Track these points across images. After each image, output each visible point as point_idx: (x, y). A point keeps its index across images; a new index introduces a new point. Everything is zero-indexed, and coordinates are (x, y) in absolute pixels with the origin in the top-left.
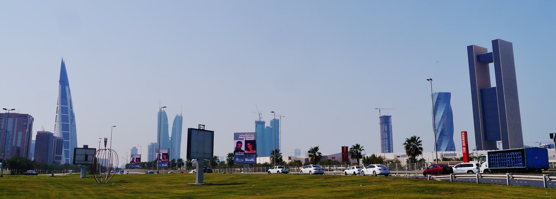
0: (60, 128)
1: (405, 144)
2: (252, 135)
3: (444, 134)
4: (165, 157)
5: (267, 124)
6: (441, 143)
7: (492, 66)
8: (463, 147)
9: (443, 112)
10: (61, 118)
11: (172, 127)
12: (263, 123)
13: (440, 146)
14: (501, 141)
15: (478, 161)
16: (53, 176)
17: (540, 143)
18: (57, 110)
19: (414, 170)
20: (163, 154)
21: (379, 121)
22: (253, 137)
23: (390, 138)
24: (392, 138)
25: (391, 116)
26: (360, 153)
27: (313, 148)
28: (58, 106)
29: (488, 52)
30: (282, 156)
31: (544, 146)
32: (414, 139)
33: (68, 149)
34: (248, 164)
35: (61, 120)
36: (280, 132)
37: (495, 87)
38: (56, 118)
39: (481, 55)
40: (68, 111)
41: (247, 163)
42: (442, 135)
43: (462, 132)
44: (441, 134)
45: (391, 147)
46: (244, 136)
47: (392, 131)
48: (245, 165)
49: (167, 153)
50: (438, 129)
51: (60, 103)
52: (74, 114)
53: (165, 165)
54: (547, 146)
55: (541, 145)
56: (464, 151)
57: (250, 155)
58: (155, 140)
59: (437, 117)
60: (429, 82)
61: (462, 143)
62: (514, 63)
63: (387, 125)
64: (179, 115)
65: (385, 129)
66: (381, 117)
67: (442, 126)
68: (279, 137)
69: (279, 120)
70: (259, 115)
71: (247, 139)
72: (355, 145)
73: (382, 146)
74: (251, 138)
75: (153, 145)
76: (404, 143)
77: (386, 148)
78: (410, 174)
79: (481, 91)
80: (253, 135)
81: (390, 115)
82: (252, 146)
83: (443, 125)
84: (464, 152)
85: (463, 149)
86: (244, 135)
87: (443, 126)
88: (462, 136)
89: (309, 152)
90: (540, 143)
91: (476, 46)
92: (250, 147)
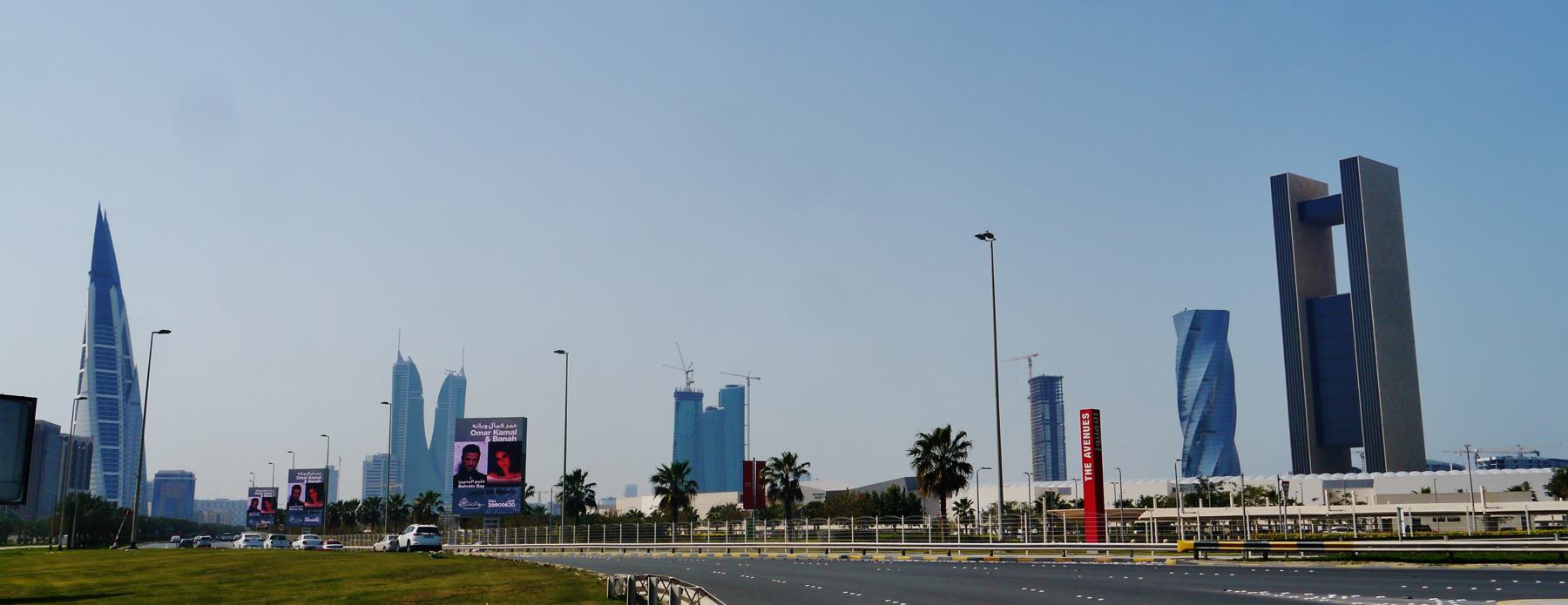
0: (90, 410)
1: (915, 452)
2: (511, 426)
3: (1209, 429)
4: (314, 495)
5: (711, 400)
6: (1201, 455)
7: (1339, 233)
8: (1085, 460)
10: (93, 382)
11: (436, 410)
12: (699, 396)
13: (1198, 464)
14: (1362, 449)
16: (395, 544)
17: (1477, 455)
18: (83, 356)
19: (504, 543)
20: (307, 484)
21: (1026, 391)
22: (515, 432)
23: (1059, 441)
24: (1064, 440)
25: (1062, 377)
26: (795, 482)
27: (669, 467)
28: (86, 345)
29: (1330, 194)
30: (593, 492)
31: (1485, 462)
32: (942, 436)
33: (115, 474)
34: (497, 515)
35: (93, 386)
36: (746, 423)
37: (1348, 295)
38: (80, 382)
39: (1311, 201)
40: (114, 359)
41: (492, 515)
42: (1204, 431)
43: (1083, 412)
44: (1201, 430)
45: (1061, 464)
46: (488, 430)
47: (1063, 418)
48: (487, 521)
49: (320, 481)
50: (1192, 413)
51: (92, 337)
52: (136, 371)
53: (314, 520)
54: (1494, 462)
55: (1478, 460)
56: (1088, 476)
57: (503, 489)
58: (381, 445)
59: (1189, 380)
60: (986, 244)
61: (1083, 449)
62: (1401, 225)
63: (1050, 404)
64: (455, 374)
65: (1043, 414)
66: (1033, 381)
67: (1204, 405)
68: (743, 434)
69: (743, 388)
70: (687, 373)
71: (495, 439)
72: (781, 458)
73: (1037, 461)
74: (507, 436)
75: (377, 460)
76: (912, 448)
77: (1046, 470)
78: (904, 554)
79: (1310, 305)
80: (515, 426)
81: (1058, 375)
82: (511, 460)
84: (1087, 479)
85: (1084, 469)
86: (486, 427)
87: (1205, 407)
88: (1082, 426)
89: (655, 479)
90: (1477, 455)
91: (1295, 178)
92: (504, 463)
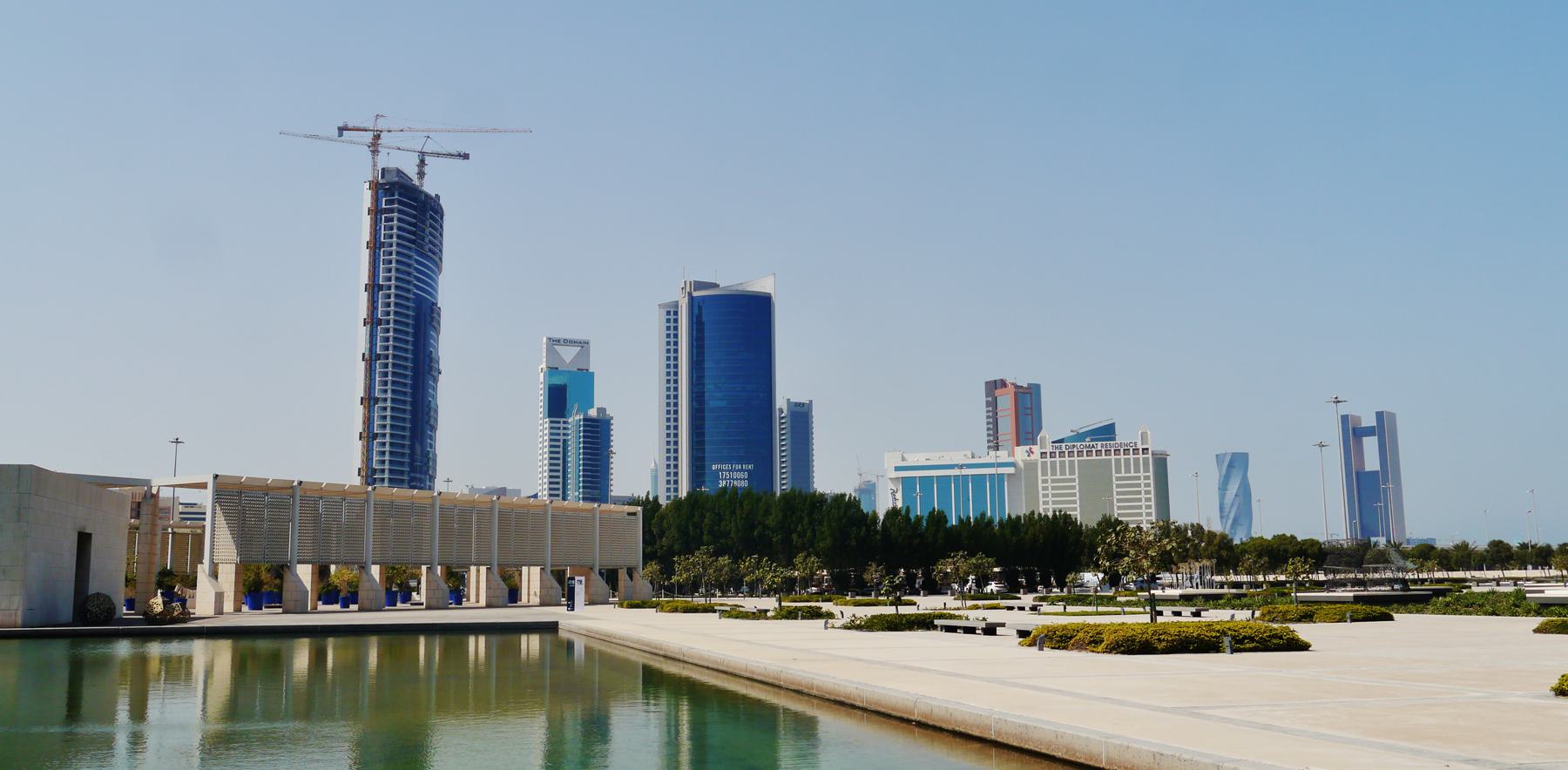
37: (1378, 472)
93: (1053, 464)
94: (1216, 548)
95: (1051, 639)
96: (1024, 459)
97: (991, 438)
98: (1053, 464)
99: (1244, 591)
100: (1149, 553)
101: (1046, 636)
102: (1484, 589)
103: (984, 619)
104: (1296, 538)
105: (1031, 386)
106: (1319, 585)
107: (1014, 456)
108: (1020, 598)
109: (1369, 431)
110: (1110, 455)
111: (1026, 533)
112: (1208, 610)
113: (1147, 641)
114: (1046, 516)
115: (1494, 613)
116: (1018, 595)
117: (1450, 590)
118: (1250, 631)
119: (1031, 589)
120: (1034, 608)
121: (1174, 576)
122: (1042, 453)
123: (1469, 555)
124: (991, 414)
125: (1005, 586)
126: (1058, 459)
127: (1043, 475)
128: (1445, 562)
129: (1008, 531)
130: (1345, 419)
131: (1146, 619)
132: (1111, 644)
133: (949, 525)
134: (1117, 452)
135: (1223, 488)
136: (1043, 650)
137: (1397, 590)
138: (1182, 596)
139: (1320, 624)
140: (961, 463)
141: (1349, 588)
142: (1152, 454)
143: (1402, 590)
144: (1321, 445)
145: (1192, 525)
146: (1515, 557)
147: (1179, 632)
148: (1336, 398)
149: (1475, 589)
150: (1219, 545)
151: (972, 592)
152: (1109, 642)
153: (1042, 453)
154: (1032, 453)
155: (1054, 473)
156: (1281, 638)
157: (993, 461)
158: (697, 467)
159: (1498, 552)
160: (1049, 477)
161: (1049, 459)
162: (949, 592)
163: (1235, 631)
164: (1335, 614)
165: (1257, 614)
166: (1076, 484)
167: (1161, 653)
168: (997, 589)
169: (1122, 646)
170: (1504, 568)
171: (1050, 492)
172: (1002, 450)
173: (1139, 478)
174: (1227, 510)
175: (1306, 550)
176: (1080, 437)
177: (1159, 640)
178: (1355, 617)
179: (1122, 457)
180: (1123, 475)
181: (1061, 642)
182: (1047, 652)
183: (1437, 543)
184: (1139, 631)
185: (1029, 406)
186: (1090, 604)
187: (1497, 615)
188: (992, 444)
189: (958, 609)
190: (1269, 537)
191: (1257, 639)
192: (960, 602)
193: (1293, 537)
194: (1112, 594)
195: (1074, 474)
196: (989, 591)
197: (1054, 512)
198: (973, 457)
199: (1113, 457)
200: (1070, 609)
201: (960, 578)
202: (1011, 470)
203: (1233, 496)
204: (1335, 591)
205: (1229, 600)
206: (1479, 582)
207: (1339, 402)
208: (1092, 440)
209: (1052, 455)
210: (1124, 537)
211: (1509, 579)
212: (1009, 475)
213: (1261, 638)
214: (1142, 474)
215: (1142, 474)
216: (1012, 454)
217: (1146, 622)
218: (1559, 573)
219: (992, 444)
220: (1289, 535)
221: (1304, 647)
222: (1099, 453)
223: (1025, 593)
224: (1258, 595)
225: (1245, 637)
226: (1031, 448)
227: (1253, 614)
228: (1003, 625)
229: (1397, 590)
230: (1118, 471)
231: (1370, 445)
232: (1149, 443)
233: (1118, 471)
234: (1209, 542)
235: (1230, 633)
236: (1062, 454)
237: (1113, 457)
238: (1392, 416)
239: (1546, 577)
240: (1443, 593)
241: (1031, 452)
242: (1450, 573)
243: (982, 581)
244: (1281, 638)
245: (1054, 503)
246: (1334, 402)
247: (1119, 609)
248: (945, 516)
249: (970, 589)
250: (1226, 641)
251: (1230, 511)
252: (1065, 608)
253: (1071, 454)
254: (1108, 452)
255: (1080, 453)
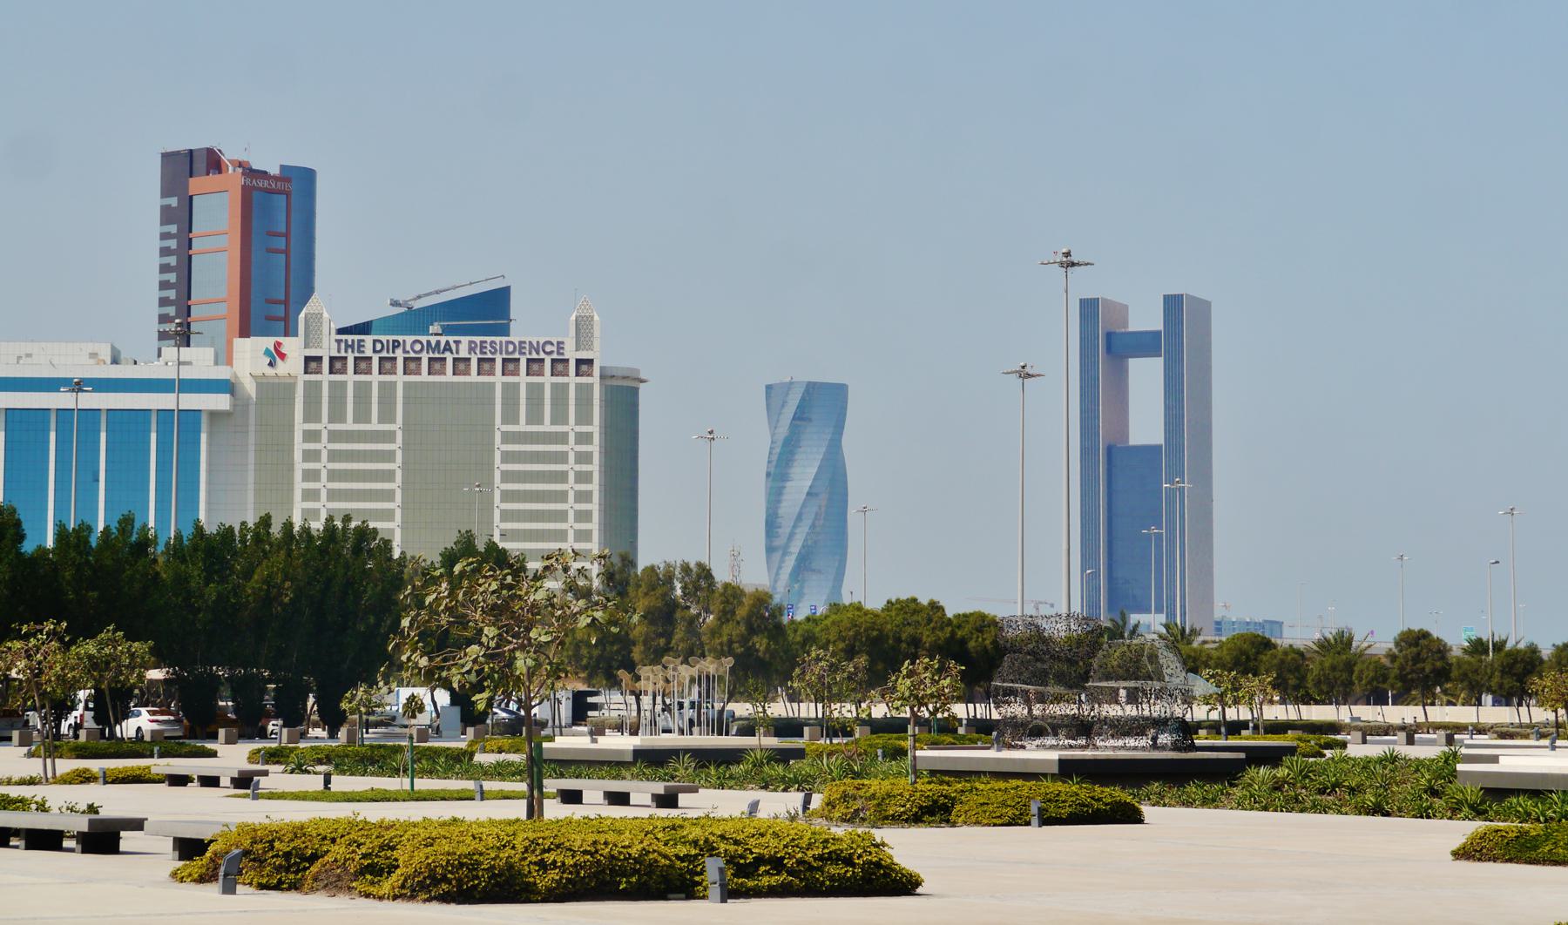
9: (817, 464)
15: (721, 712)
37: (1157, 448)
79: (1110, 450)
83: (813, 526)
93: (338, 390)
94: (742, 628)
95: (260, 861)
96: (258, 372)
97: (171, 311)
98: (338, 390)
99: (732, 741)
100: (533, 634)
101: (246, 853)
102: (1374, 750)
103: (92, 809)
104: (941, 609)
105: (288, 174)
106: (983, 729)
107: (229, 362)
108: (213, 754)
109: (1146, 344)
110: (491, 373)
111: (248, 575)
112: (695, 790)
113: (510, 867)
114: (306, 531)
115: (1378, 810)
116: (210, 746)
117: (1291, 751)
118: (773, 843)
119: (248, 727)
120: (243, 781)
121: (631, 699)
122: (308, 360)
123: (1349, 666)
124: (173, 244)
125: (178, 721)
126: (350, 377)
127: (306, 420)
128: (1292, 682)
129: (195, 572)
130: (1089, 308)
131: (518, 809)
132: (417, 873)
133: (28, 547)
134: (510, 365)
135: (778, 474)
136: (233, 892)
137: (1163, 748)
138: (640, 755)
139: (965, 828)
140: (77, 374)
141: (1050, 741)
142: (602, 377)
143: (1176, 747)
144: (1023, 374)
145: (686, 569)
146: (1455, 674)
147: (595, 843)
148: (1068, 254)
149: (1356, 750)
150: (748, 621)
151: (83, 734)
152: (410, 870)
153: (308, 360)
154: (282, 356)
155: (337, 415)
156: (848, 861)
157: (169, 373)
158: (419, 331)
159: (1417, 658)
160: (324, 425)
161: (325, 377)
162: (15, 734)
163: (736, 842)
164: (1004, 804)
165: (817, 801)
166: (396, 446)
167: (545, 900)
168: (155, 726)
169: (444, 879)
170: (1428, 699)
171: (324, 465)
172: (198, 345)
173: (562, 438)
174: (785, 531)
175: (963, 642)
176: (415, 320)
177: (542, 865)
178: (1053, 811)
179: (523, 379)
180: (522, 427)
181: (287, 871)
182: (248, 898)
183: (1286, 632)
184: (491, 841)
185: (283, 229)
186: (395, 772)
187: (1387, 814)
188: (170, 327)
189: (31, 782)
190: (875, 603)
191: (789, 863)
192: (39, 761)
193: (935, 607)
194: (463, 745)
195: (393, 421)
196: (132, 733)
197: (330, 519)
198: (115, 361)
199: (498, 379)
200: (341, 783)
201: (43, 695)
202: (221, 402)
203: (803, 496)
204: (1023, 747)
205: (758, 765)
206: (1369, 732)
207: (1073, 264)
208: (447, 331)
209: (337, 364)
210: (470, 593)
211: (1437, 727)
212: (214, 415)
213: (800, 862)
214: (571, 427)
215: (571, 427)
216: (225, 357)
217: (513, 817)
218: (1551, 716)
219: (170, 327)
220: (924, 601)
221: (905, 885)
222: (462, 366)
223: (229, 741)
224: (830, 755)
225: (760, 860)
226: (278, 345)
227: (807, 802)
228: (137, 825)
229: (1163, 748)
230: (510, 416)
231: (1145, 375)
232: (597, 344)
233: (510, 416)
234: (724, 612)
235: (722, 847)
236: (362, 364)
237: (498, 379)
238: (1203, 308)
239: (1521, 725)
240: (1271, 757)
241: (278, 354)
242: (1303, 708)
243: (111, 706)
244: (848, 861)
245: (333, 495)
246: (1062, 264)
247: (470, 785)
248: (18, 524)
249: (77, 727)
250: (712, 868)
251: (791, 536)
252: (327, 782)
253: (387, 365)
254: (485, 364)
255: (411, 365)
